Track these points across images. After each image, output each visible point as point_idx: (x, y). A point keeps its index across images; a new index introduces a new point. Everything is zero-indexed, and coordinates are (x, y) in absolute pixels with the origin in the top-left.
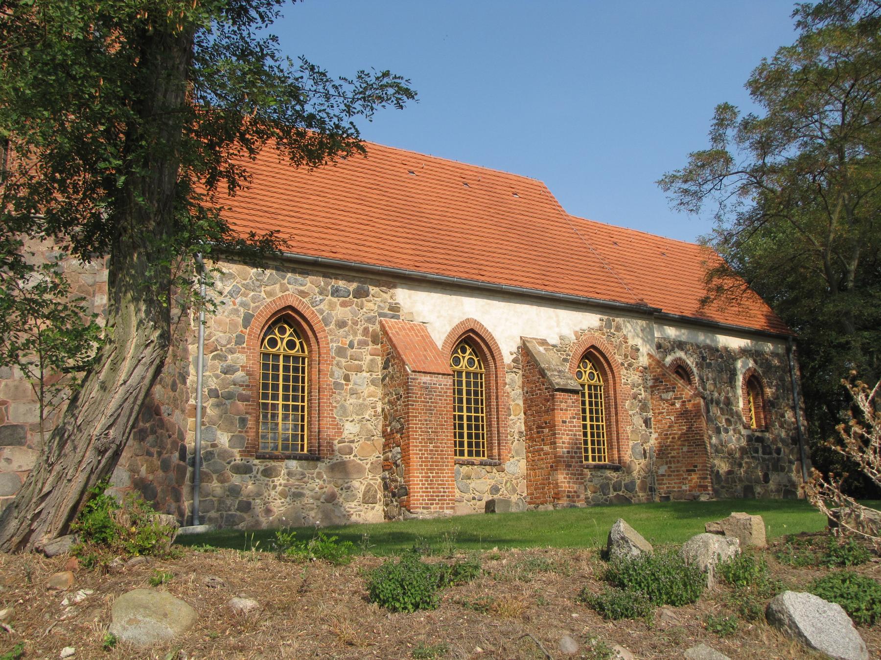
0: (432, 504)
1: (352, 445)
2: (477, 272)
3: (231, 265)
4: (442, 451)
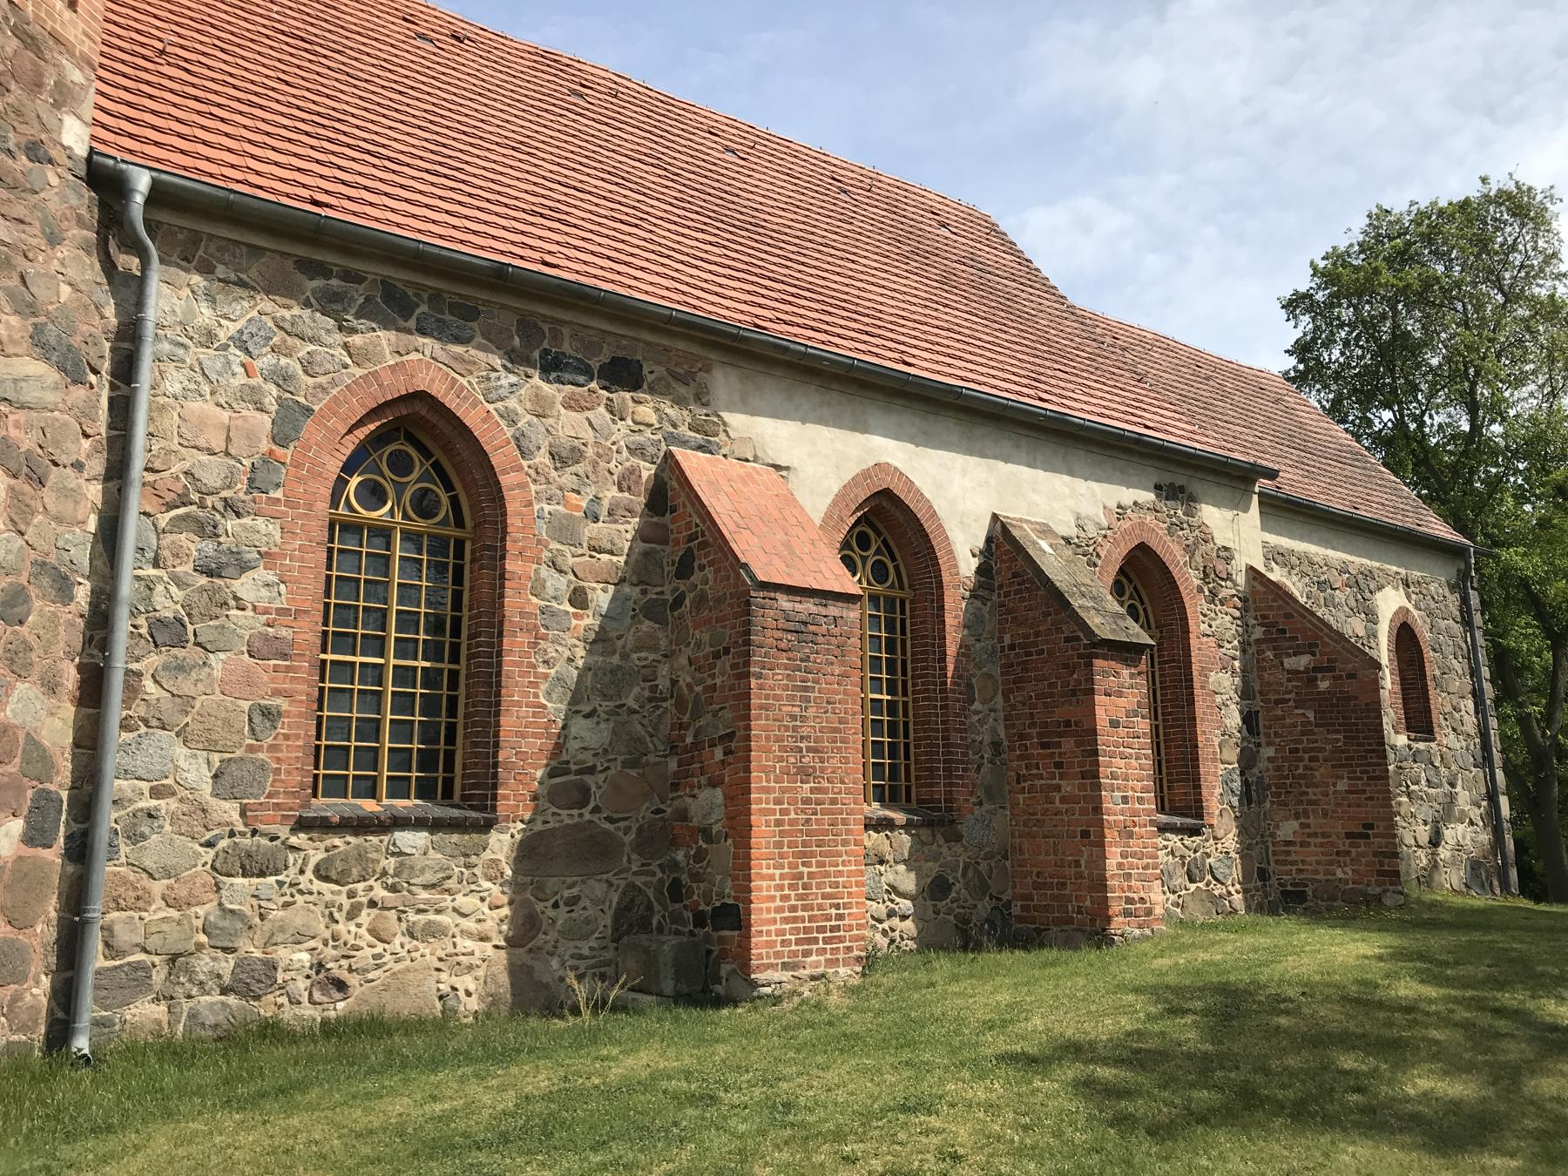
0: (807, 954)
1: (589, 779)
2: (897, 356)
3: (518, 603)
4: (833, 801)
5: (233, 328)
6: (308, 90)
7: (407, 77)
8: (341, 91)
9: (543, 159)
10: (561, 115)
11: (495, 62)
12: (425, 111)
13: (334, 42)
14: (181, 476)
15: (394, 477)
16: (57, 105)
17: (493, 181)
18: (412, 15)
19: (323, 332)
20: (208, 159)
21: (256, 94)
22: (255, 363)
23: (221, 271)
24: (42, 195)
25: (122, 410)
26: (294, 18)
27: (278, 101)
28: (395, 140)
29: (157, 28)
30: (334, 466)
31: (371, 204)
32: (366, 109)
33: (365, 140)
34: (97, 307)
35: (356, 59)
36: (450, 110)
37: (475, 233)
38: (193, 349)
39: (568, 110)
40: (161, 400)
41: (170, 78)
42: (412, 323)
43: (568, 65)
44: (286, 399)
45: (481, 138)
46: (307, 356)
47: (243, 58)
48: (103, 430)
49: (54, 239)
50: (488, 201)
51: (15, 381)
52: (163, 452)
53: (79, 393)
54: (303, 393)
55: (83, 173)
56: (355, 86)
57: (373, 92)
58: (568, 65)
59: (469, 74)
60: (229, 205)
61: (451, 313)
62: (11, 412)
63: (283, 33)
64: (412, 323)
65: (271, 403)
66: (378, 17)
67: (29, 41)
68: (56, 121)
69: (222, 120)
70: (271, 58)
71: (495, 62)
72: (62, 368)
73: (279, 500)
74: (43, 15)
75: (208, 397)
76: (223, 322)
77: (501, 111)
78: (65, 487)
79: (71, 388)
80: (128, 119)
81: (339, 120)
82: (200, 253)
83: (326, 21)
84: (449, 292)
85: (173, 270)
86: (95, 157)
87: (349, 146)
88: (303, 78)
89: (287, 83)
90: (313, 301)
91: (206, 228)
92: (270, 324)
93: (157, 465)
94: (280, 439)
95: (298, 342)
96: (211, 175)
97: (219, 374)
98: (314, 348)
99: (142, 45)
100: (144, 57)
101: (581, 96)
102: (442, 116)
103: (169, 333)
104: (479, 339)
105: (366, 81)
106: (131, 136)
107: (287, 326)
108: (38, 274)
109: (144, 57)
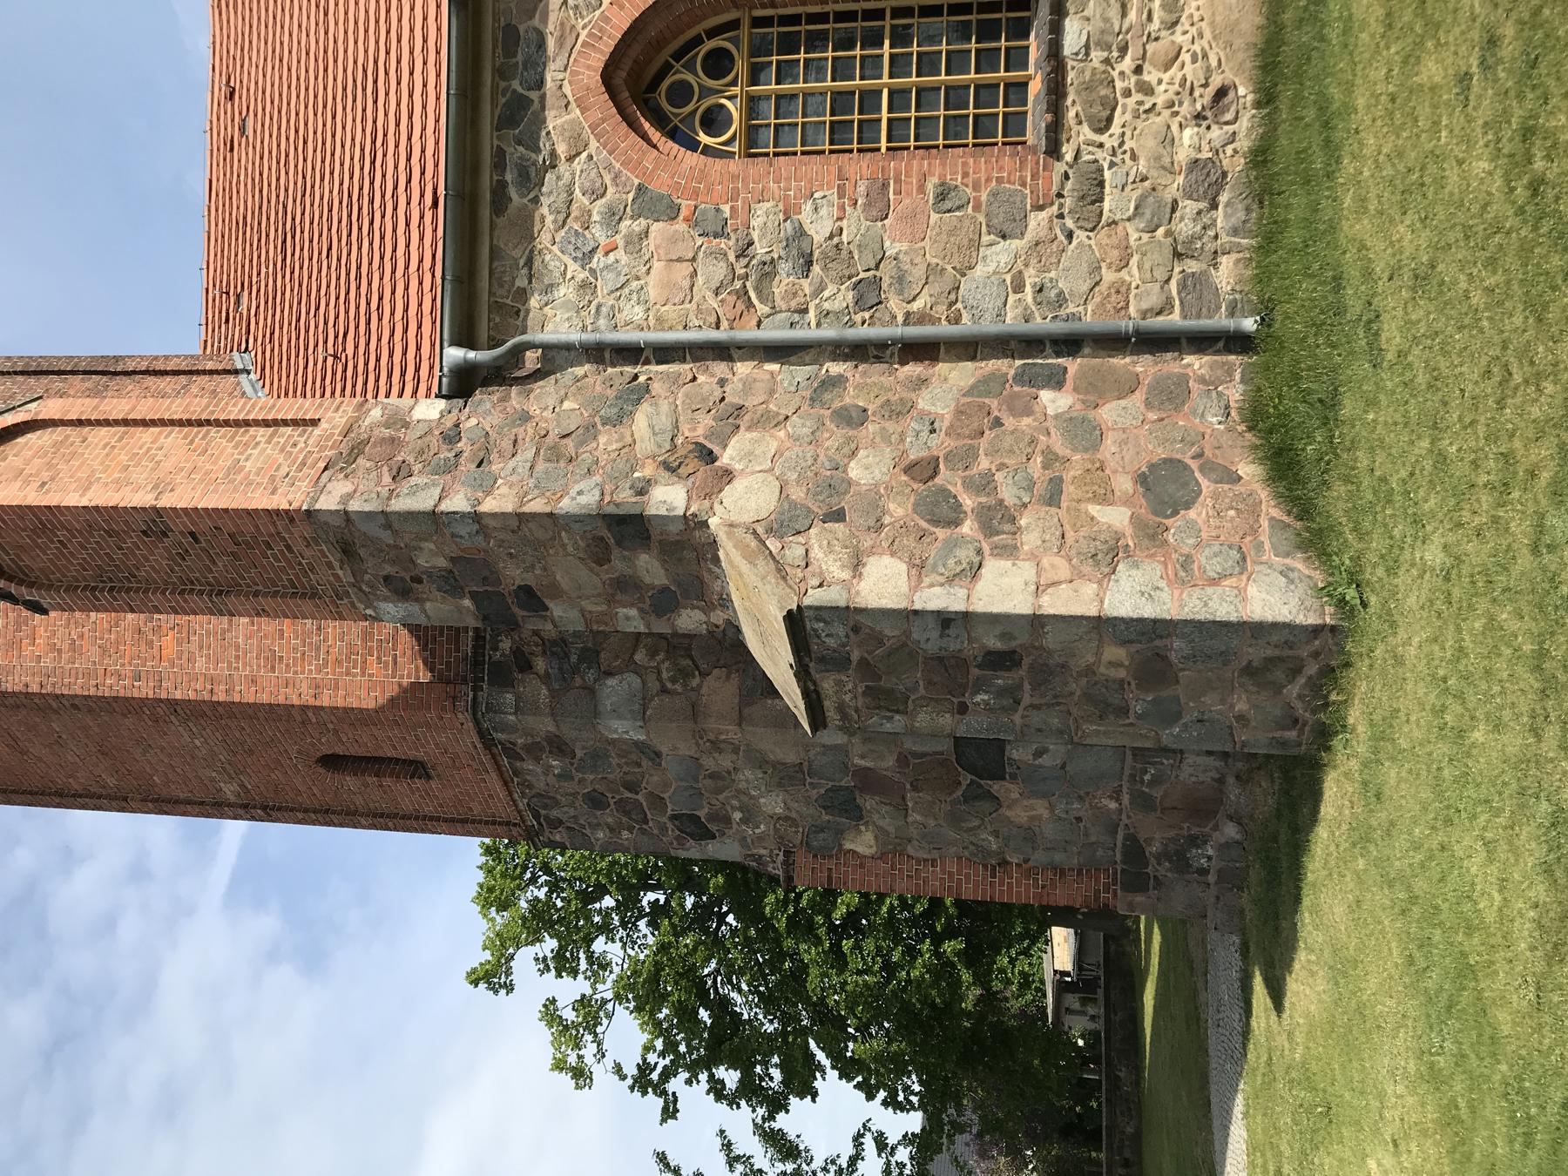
5: (573, 267)
7: (287, 139)
8: (322, 198)
12: (315, 115)
16: (406, 425)
19: (561, 183)
20: (420, 305)
21: (348, 274)
23: (521, 282)
25: (666, 353)
27: (349, 254)
28: (353, 139)
29: (315, 364)
30: (692, 159)
31: (423, 151)
32: (332, 173)
37: (425, 41)
40: (652, 322)
41: (356, 347)
42: (534, 95)
47: (319, 291)
48: (687, 367)
49: (525, 417)
50: (388, 32)
51: (655, 434)
53: (656, 387)
55: (461, 401)
60: (457, 280)
61: (515, 55)
63: (284, 260)
64: (534, 95)
65: (639, 225)
66: (238, 176)
67: (356, 451)
69: (381, 298)
71: (242, 50)
72: (638, 401)
75: (642, 282)
76: (569, 276)
80: (403, 374)
81: (350, 196)
82: (509, 302)
83: (259, 224)
85: (529, 323)
87: (372, 183)
88: (320, 235)
89: (330, 249)
90: (532, 195)
92: (562, 233)
93: (713, 319)
94: (672, 213)
95: (574, 206)
97: (619, 274)
99: (334, 374)
100: (345, 371)
103: (589, 321)
104: (536, 22)
106: (417, 370)
107: (561, 217)
108: (558, 425)
109: (345, 371)
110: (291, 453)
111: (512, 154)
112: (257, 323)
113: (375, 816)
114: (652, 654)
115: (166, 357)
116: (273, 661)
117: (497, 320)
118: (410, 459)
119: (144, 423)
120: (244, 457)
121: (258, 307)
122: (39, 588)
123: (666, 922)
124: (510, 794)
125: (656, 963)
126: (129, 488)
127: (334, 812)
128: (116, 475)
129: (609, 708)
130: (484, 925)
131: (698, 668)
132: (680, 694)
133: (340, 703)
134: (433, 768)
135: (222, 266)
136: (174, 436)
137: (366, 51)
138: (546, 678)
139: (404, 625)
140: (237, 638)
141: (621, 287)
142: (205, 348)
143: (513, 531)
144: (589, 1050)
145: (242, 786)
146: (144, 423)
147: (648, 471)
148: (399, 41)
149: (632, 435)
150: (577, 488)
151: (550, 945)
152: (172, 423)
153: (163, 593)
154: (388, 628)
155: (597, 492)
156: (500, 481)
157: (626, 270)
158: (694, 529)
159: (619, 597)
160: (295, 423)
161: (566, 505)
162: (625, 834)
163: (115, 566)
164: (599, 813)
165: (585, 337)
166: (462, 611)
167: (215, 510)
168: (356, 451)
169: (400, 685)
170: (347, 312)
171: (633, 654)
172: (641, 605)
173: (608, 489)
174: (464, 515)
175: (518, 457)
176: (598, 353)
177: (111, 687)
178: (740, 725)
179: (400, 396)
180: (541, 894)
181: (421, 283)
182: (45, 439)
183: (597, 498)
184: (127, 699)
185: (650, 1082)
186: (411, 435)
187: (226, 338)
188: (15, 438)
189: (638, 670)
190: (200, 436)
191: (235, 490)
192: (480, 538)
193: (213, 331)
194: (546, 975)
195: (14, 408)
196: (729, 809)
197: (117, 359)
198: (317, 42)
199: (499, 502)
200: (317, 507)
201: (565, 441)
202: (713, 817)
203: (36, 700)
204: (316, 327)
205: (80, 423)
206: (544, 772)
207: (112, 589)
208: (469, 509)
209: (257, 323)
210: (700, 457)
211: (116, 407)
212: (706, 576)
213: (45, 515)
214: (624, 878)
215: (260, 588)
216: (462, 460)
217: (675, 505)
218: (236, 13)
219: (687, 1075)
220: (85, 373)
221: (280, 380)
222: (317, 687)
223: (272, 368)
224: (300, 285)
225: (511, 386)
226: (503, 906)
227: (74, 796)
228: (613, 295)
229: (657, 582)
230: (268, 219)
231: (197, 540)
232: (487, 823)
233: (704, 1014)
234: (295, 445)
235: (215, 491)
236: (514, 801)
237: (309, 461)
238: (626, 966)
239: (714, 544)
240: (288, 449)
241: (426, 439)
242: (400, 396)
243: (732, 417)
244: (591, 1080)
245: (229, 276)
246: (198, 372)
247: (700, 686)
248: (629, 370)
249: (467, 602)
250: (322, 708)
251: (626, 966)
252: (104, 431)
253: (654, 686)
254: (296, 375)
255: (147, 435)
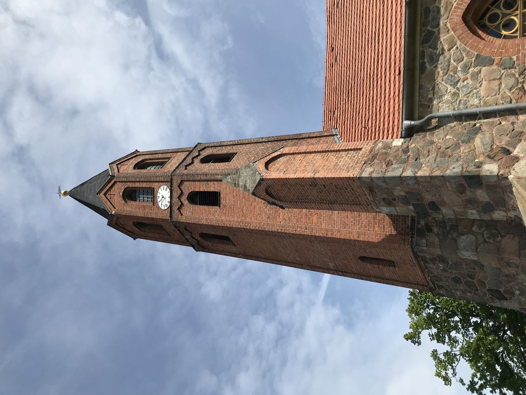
5: (450, 88)
6: (363, 87)
7: (350, 60)
8: (361, 77)
9: (363, 7)
10: (346, 7)
11: (336, 35)
12: (359, 51)
13: (346, 84)
14: (512, 91)
15: (500, 18)
16: (390, 148)
17: (376, 21)
18: (331, 65)
19: (446, 59)
20: (394, 108)
21: (369, 100)
22: (462, 78)
23: (430, 96)
24: (419, 147)
25: (487, 115)
26: (343, 97)
27: (370, 94)
28: (371, 57)
29: (358, 131)
30: (499, 41)
31: (395, 56)
32: (364, 69)
33: (374, 66)
34: (452, 128)
35: (349, 76)
36: (356, 43)
37: (396, 19)
38: (461, 98)
39: (344, 6)
40: (482, 103)
41: (372, 124)
42: (436, 30)
43: (329, 12)
44: (474, 64)
45: (362, 30)
46: (456, 62)
47: (359, 107)
48: (497, 119)
49: (432, 142)
50: (383, 20)
51: (484, 145)
52: (503, 99)
53: (484, 128)
54: (471, 60)
55: (409, 139)
56: (358, 74)
57: (358, 68)
58: (329, 12)
59: (343, 42)
60: (408, 98)
61: (429, 17)
62: (496, 145)
63: (348, 98)
64: (436, 30)
65: (476, 70)
66: (334, 74)
67: (374, 157)
68: (395, 148)
69: (380, 107)
70: (357, 99)
71: (336, 35)
72: (476, 133)
73: (517, 57)
74: (365, 155)
75: (478, 90)
76: (448, 91)
77: (351, 28)
78: (522, 126)
79: (483, 130)
80: (388, 131)
81: (370, 75)
82: (426, 103)
83: (341, 88)
84: (421, 20)
85: (433, 110)
86: (403, 136)
87: (377, 70)
88: (360, 89)
89: (363, 93)
90: (434, 65)
91: (417, 103)
92: (446, 77)
93: (509, 100)
94: (491, 62)
95: (451, 66)
96: (399, 106)
97: (468, 88)
98: (452, 61)
99: (364, 133)
100: (368, 132)
101: (338, 4)
102: (359, 45)
103: (456, 107)
104: (437, 4)
105: (355, 71)
106: (393, 129)
107: (445, 71)
108: (445, 145)
109: (368, 132)
110: (353, 159)
111: (427, 52)
112: (340, 120)
113: (377, 278)
114: (480, 227)
115: (313, 133)
116: (345, 225)
117: (422, 110)
118: (392, 159)
119: (310, 153)
120: (339, 161)
121: (340, 114)
122: (283, 202)
123: (481, 329)
124: (424, 275)
125: (477, 344)
126: (307, 172)
127: (363, 275)
128: (303, 168)
129: (462, 247)
130: (410, 320)
131: (500, 234)
132: (492, 243)
133: (366, 240)
134: (397, 263)
135: (329, 103)
136: (318, 156)
137: (376, 28)
138: (438, 235)
139: (387, 214)
140: (334, 217)
141: (470, 93)
142: (324, 129)
143: (428, 182)
144: (450, 372)
145: (335, 264)
146: (310, 153)
147: (481, 159)
148: (387, 22)
149: (474, 146)
150: (452, 166)
151: (434, 330)
152: (318, 152)
153: (315, 203)
154: (382, 215)
155: (460, 168)
156: (424, 165)
157: (471, 86)
158: (502, 180)
159: (469, 206)
160: (354, 150)
161: (448, 172)
162: (469, 294)
163: (302, 195)
164: (458, 285)
165: (455, 112)
166: (409, 210)
167: (331, 178)
168: (374, 157)
169: (386, 235)
170: (369, 113)
171: (472, 227)
172: (478, 209)
173: (465, 166)
174: (411, 177)
175: (430, 157)
176: (459, 118)
177: (299, 231)
178: (519, 257)
179: (387, 138)
180: (431, 311)
181: (394, 100)
182: (285, 159)
183: (461, 170)
184: (303, 235)
185: (475, 389)
186: (391, 152)
187: (330, 125)
188: (277, 159)
189: (474, 233)
190: (326, 155)
191: (337, 171)
192: (417, 185)
193: (326, 123)
194: (433, 341)
195: (277, 151)
196: (514, 289)
197: (300, 134)
198: (359, 28)
199: (423, 172)
200: (362, 176)
201: (447, 150)
202: (505, 292)
203: (280, 234)
204: (359, 119)
205: (293, 154)
206: (437, 268)
207: (301, 202)
208: (413, 175)
209: (340, 120)
210: (504, 153)
211: (303, 148)
212: (507, 198)
213: (276, 181)
214: (463, 310)
215: (343, 202)
216: (410, 159)
217: (493, 171)
218: (334, 24)
219: (491, 389)
220: (292, 139)
221: (347, 137)
222: (359, 234)
223: (344, 133)
224: (354, 106)
225: (427, 132)
226: (417, 314)
227: (289, 263)
228: (466, 96)
229: (485, 200)
230: (343, 86)
231: (325, 187)
232: (415, 284)
233: (498, 368)
234: (354, 157)
235: (331, 172)
236: (425, 278)
237: (359, 162)
238: (464, 343)
239: (510, 186)
240: (352, 158)
241: (397, 152)
242: (387, 138)
243: (518, 137)
244: (451, 383)
245: (331, 106)
246: (322, 136)
247: (501, 241)
248: (472, 122)
249: (411, 207)
250: (360, 241)
251: (464, 343)
252: (299, 156)
253: (481, 240)
254: (352, 134)
255: (311, 156)
